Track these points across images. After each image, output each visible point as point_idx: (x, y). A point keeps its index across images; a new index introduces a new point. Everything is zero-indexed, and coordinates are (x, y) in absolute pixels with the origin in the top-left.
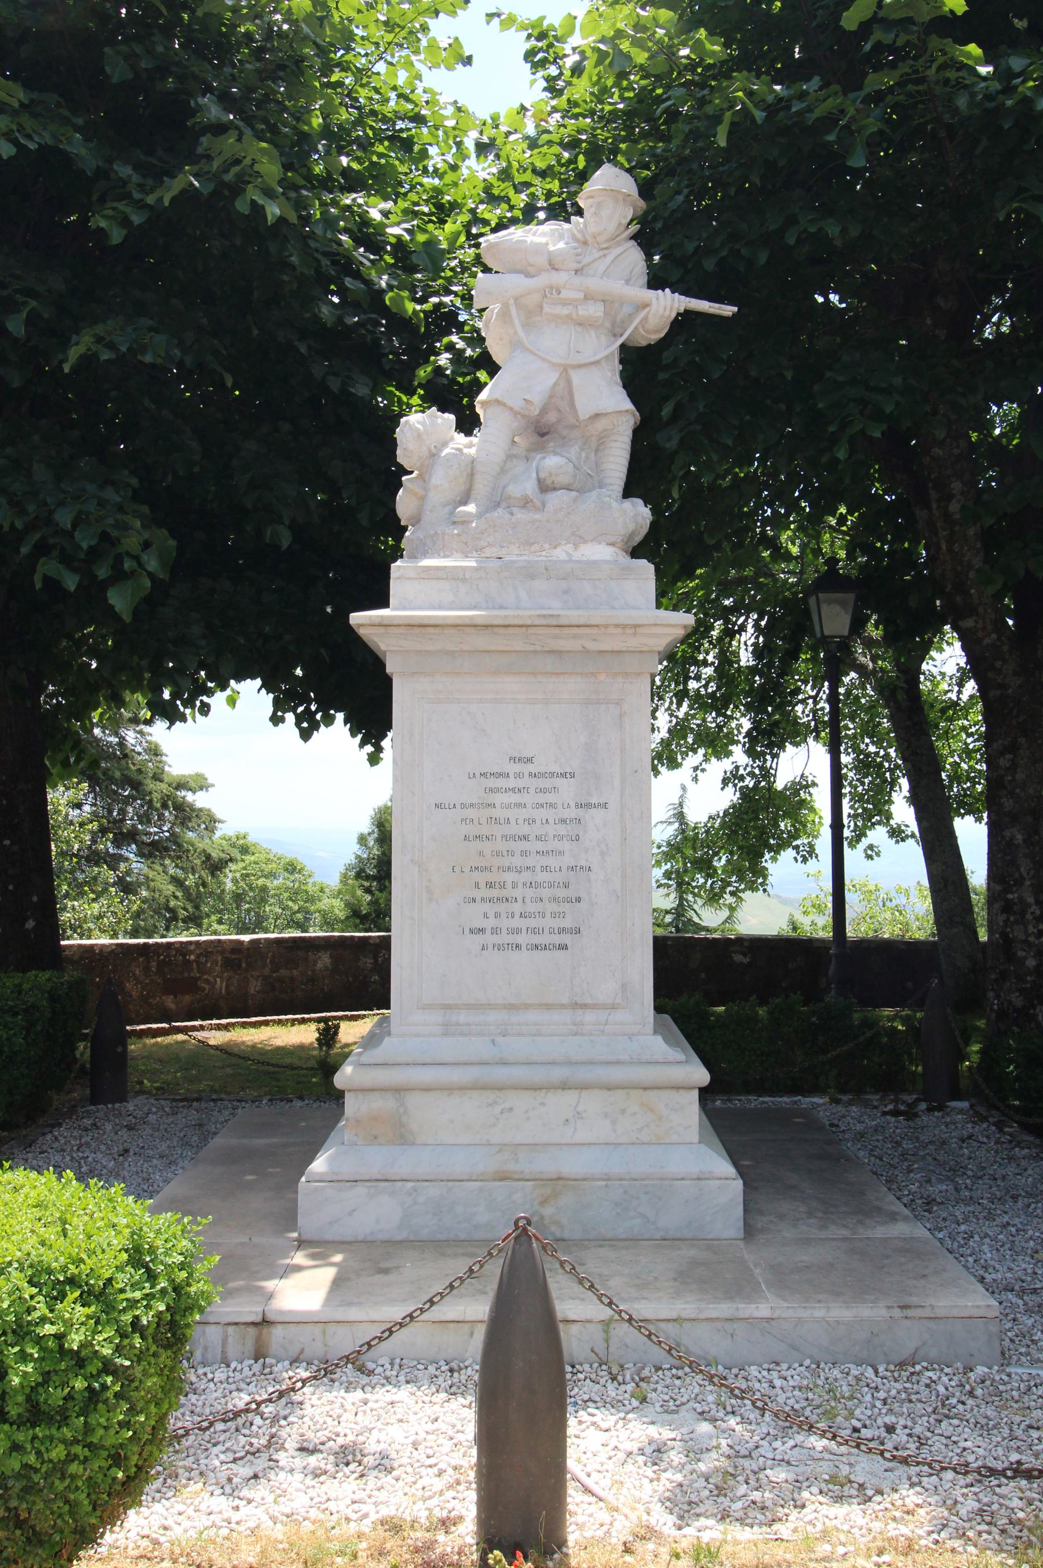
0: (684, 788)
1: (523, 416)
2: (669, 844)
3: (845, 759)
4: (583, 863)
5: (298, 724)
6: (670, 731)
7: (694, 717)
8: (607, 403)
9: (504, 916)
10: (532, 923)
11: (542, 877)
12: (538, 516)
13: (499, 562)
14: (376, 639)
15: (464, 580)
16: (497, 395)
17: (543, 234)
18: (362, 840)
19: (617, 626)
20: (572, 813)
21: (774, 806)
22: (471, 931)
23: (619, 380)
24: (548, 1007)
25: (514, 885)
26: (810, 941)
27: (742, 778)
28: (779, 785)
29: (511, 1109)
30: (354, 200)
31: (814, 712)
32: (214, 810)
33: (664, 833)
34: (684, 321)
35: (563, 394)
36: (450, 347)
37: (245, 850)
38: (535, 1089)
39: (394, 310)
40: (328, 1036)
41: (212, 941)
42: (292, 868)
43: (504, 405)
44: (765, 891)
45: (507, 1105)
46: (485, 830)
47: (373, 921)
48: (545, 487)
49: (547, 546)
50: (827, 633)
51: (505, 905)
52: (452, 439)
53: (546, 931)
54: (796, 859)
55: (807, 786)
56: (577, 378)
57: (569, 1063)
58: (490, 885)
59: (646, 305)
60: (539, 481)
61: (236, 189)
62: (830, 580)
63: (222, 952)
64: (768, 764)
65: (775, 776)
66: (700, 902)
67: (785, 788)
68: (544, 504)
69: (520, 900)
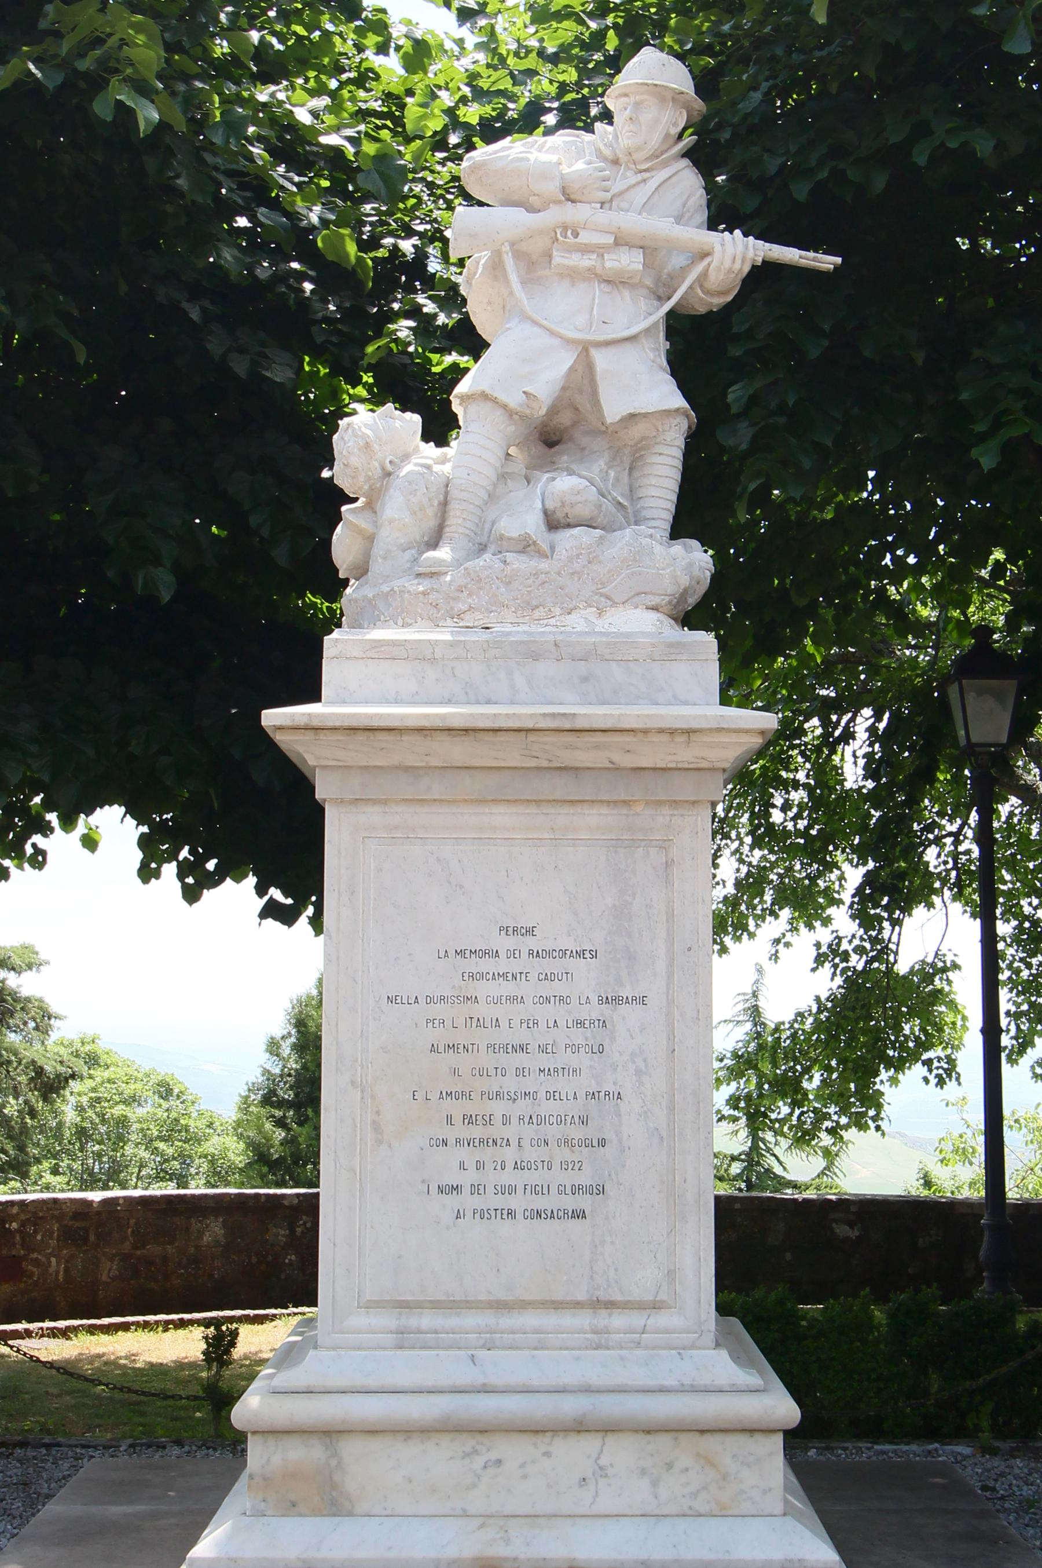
0: (760, 971)
1: (523, 417)
2: (735, 1055)
3: (1004, 929)
4: (611, 1088)
5: (181, 876)
6: (738, 884)
7: (774, 865)
8: (645, 390)
9: (490, 1166)
10: (532, 1177)
11: (548, 1107)
12: (544, 565)
13: (485, 636)
14: (301, 749)
15: (433, 661)
16: (484, 387)
17: (554, 150)
18: (273, 1047)
19: (661, 731)
20: (595, 1011)
21: (895, 998)
22: (440, 1190)
23: (665, 363)
24: (556, 1305)
25: (506, 1120)
26: (952, 1206)
27: (845, 956)
28: (902, 968)
29: (499, 1462)
30: (273, 95)
31: (955, 855)
32: (47, 1000)
33: (729, 1038)
34: (762, 275)
35: (583, 381)
36: (413, 311)
37: (92, 1060)
38: (536, 1432)
39: (330, 257)
40: (220, 1347)
41: (44, 1201)
42: (165, 1090)
43: (494, 401)
44: (878, 1128)
45: (493, 1455)
46: (462, 1038)
47: (288, 1171)
48: (553, 523)
49: (557, 611)
50: (974, 739)
51: (492, 1149)
52: (416, 450)
53: (554, 1189)
54: (926, 1080)
55: (944, 970)
56: (601, 359)
57: (588, 1390)
58: (469, 1120)
59: (705, 255)
60: (546, 513)
61: (97, 83)
62: (981, 659)
63: (59, 1219)
64: (886, 934)
65: (896, 953)
66: (785, 1143)
67: (912, 972)
68: (553, 548)
69: (514, 1143)
